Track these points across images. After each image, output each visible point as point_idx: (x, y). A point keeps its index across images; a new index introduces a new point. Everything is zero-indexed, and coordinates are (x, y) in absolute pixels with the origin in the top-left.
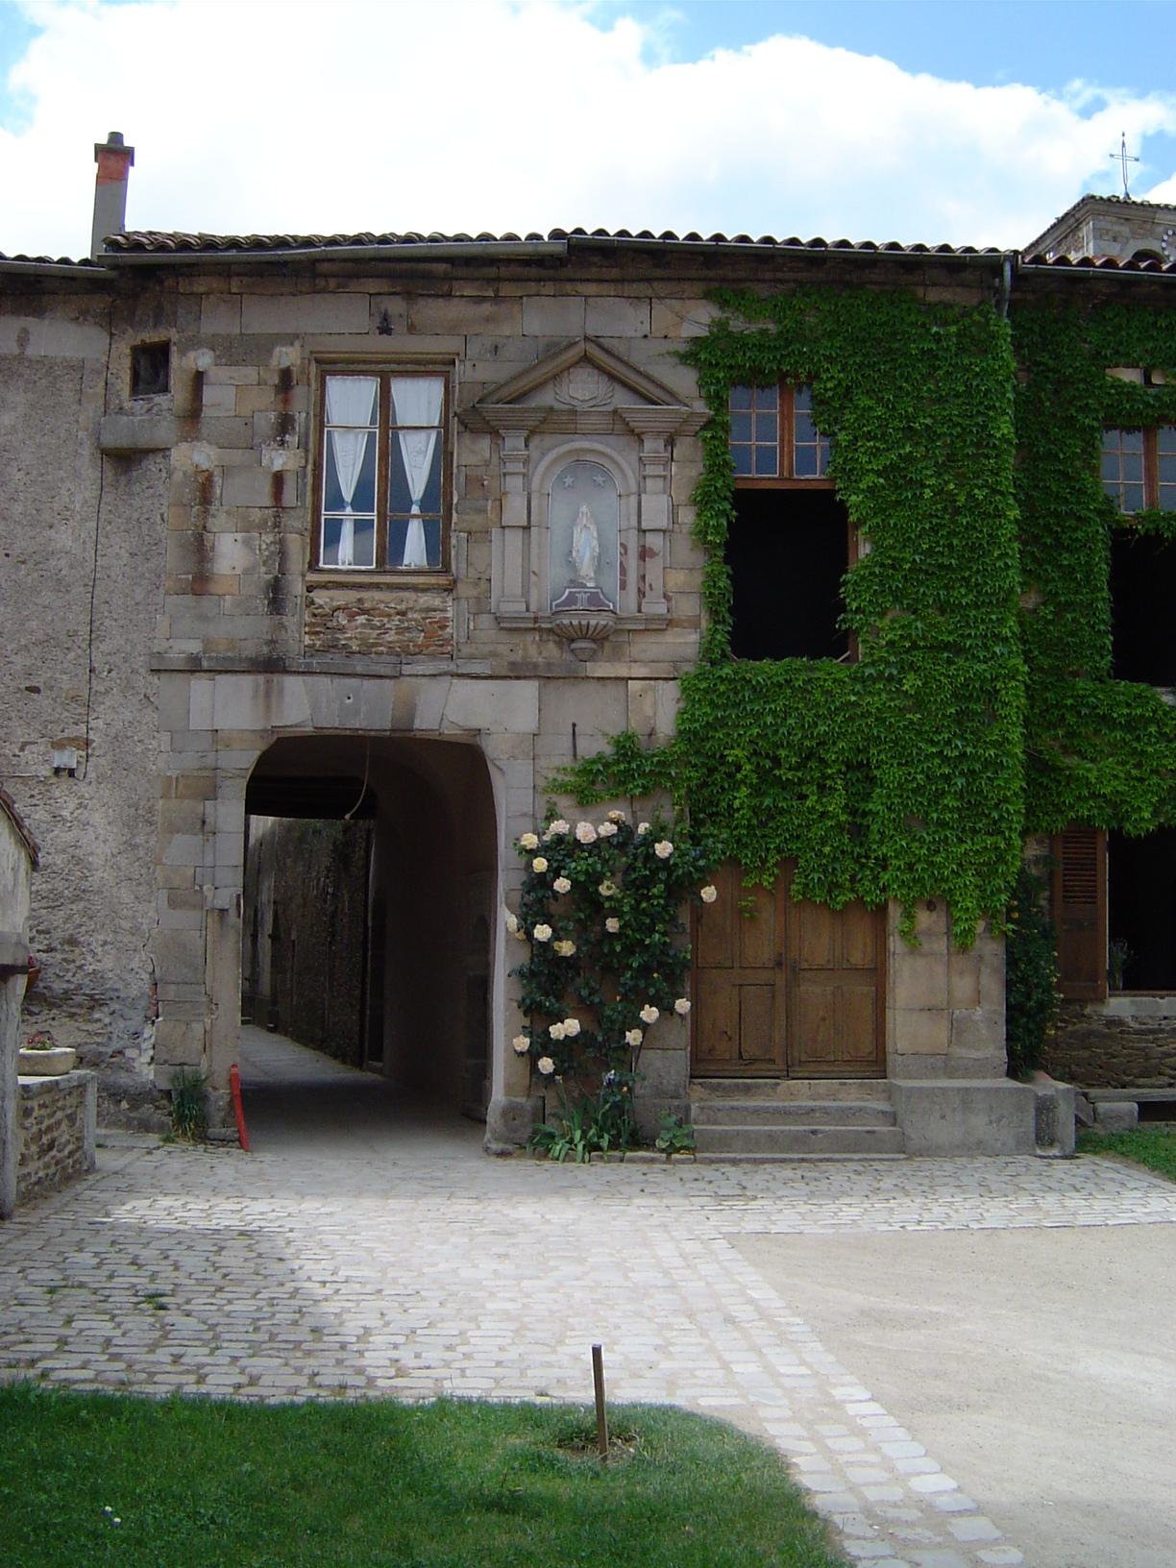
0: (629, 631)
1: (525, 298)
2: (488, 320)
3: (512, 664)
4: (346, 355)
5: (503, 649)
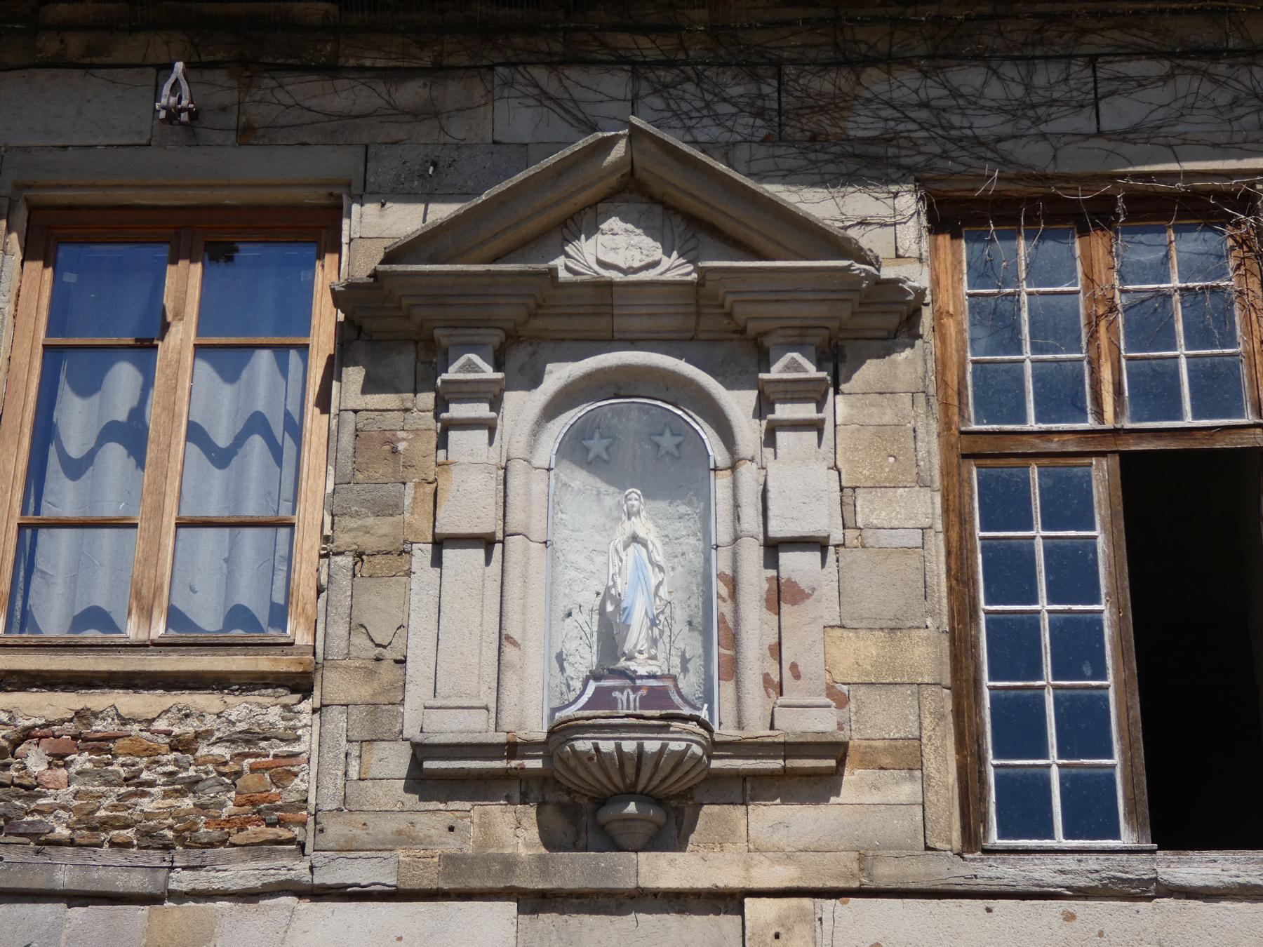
3: (452, 861)
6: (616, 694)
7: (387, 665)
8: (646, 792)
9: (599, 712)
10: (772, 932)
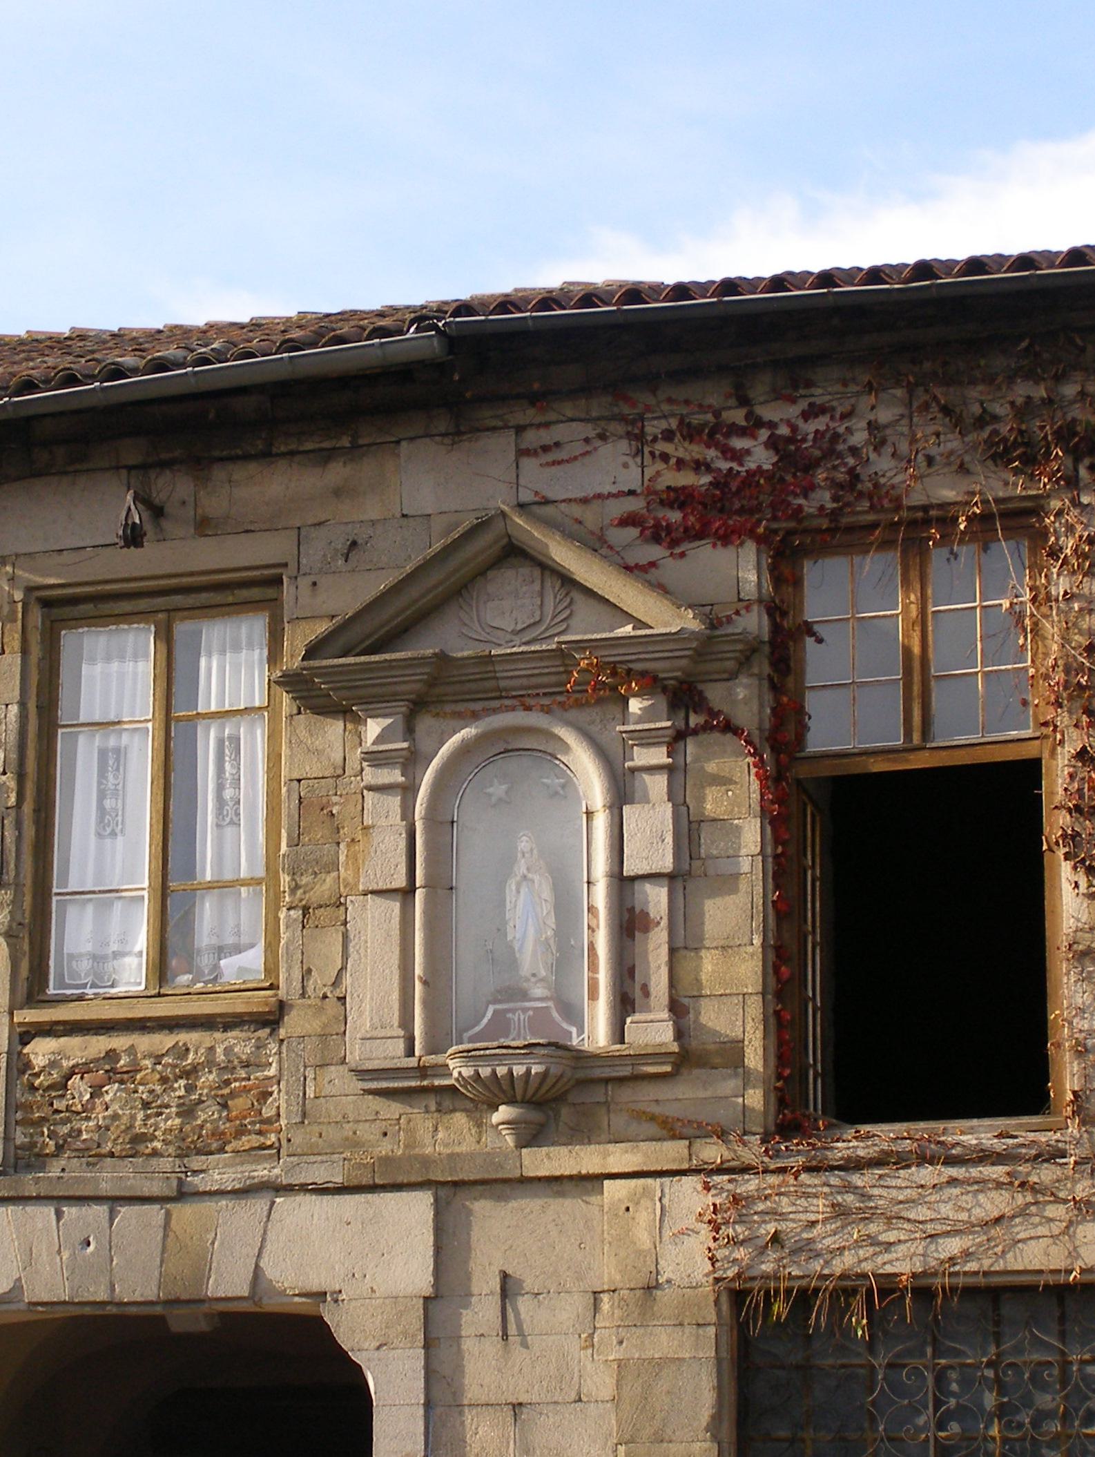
0: (607, 1081)
1: (404, 444)
2: (338, 493)
3: (387, 1161)
4: (266, 572)
5: (368, 1132)
6: (510, 1015)
7: (332, 1000)
8: (527, 1098)
9: (478, 1045)
10: (623, 1208)
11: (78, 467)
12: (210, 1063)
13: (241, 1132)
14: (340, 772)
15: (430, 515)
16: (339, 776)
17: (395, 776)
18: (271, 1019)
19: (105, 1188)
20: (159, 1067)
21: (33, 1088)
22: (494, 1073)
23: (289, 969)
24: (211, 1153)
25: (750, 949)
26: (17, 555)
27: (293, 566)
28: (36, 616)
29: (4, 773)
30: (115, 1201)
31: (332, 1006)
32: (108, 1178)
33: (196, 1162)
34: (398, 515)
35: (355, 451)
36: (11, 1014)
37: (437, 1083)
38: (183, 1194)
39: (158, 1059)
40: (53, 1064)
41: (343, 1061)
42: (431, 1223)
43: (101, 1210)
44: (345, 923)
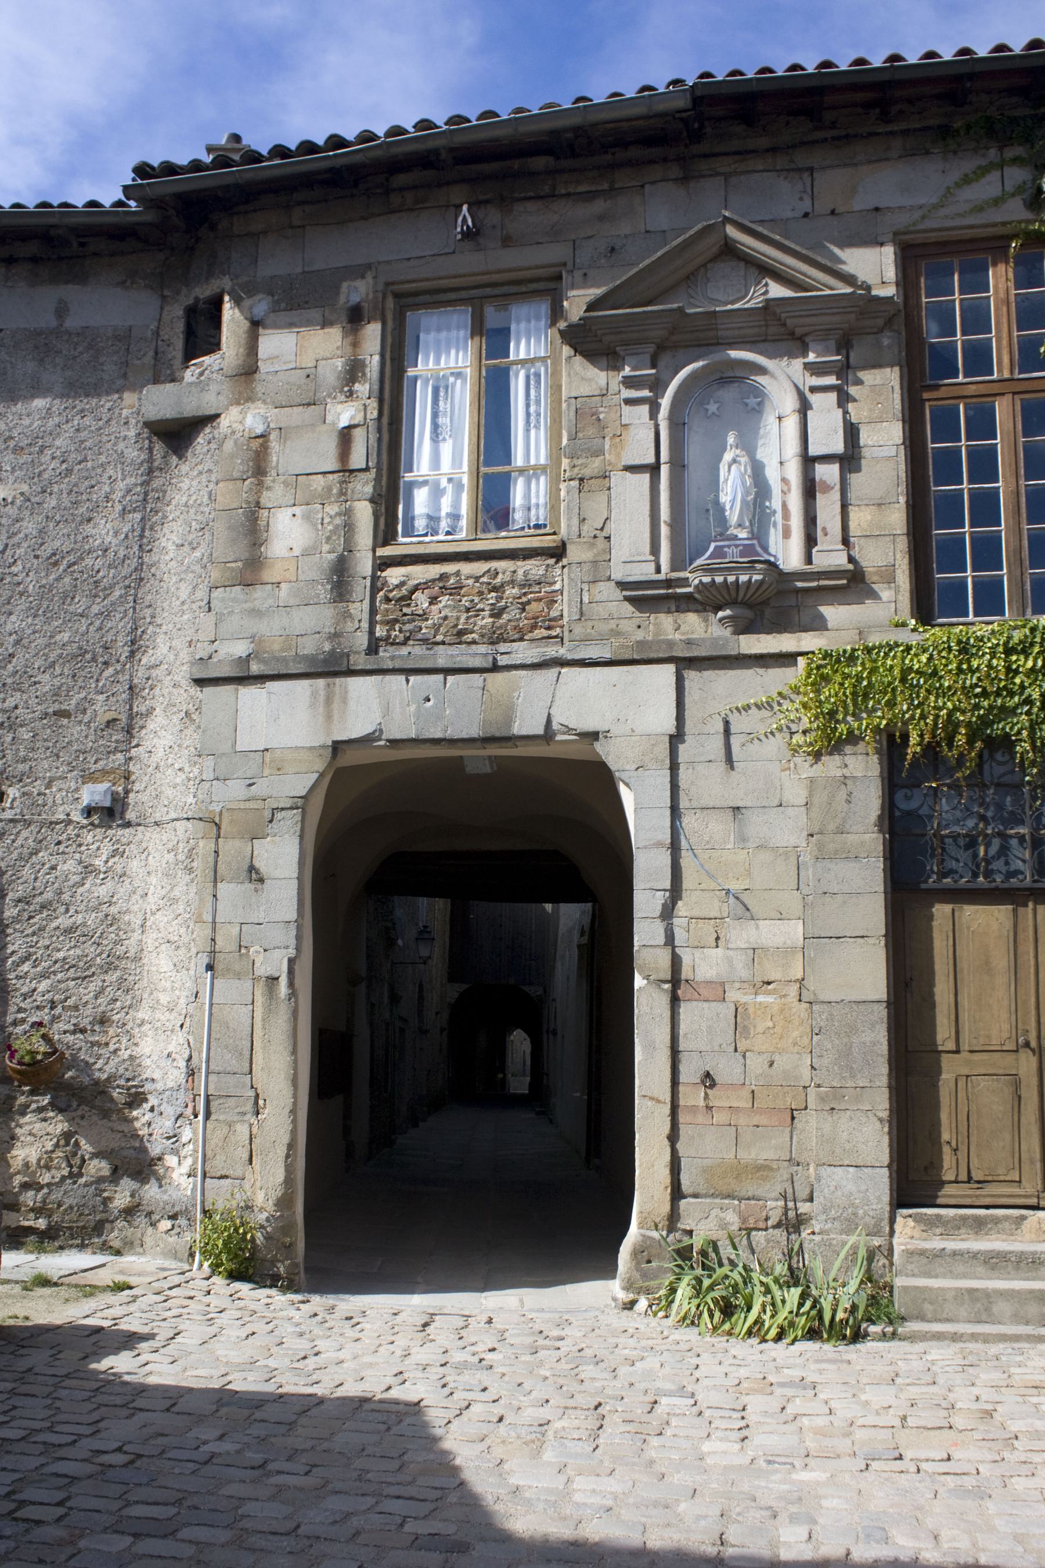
1: (647, 187)
2: (602, 218)
3: (641, 644)
5: (627, 626)
11: (421, 206)
12: (512, 582)
13: (534, 627)
14: (605, 392)
15: (664, 231)
16: (603, 395)
17: (646, 393)
18: (558, 552)
19: (441, 662)
20: (478, 585)
21: (388, 600)
22: (725, 580)
23: (569, 519)
24: (514, 641)
25: (897, 506)
26: (379, 263)
27: (570, 266)
28: (390, 303)
29: (369, 398)
30: (448, 671)
31: (601, 543)
32: (443, 657)
33: (503, 647)
34: (643, 231)
35: (612, 191)
36: (374, 551)
37: (679, 590)
38: (495, 668)
39: (477, 579)
40: (403, 584)
41: (609, 579)
42: (674, 686)
43: (440, 677)
44: (609, 489)
